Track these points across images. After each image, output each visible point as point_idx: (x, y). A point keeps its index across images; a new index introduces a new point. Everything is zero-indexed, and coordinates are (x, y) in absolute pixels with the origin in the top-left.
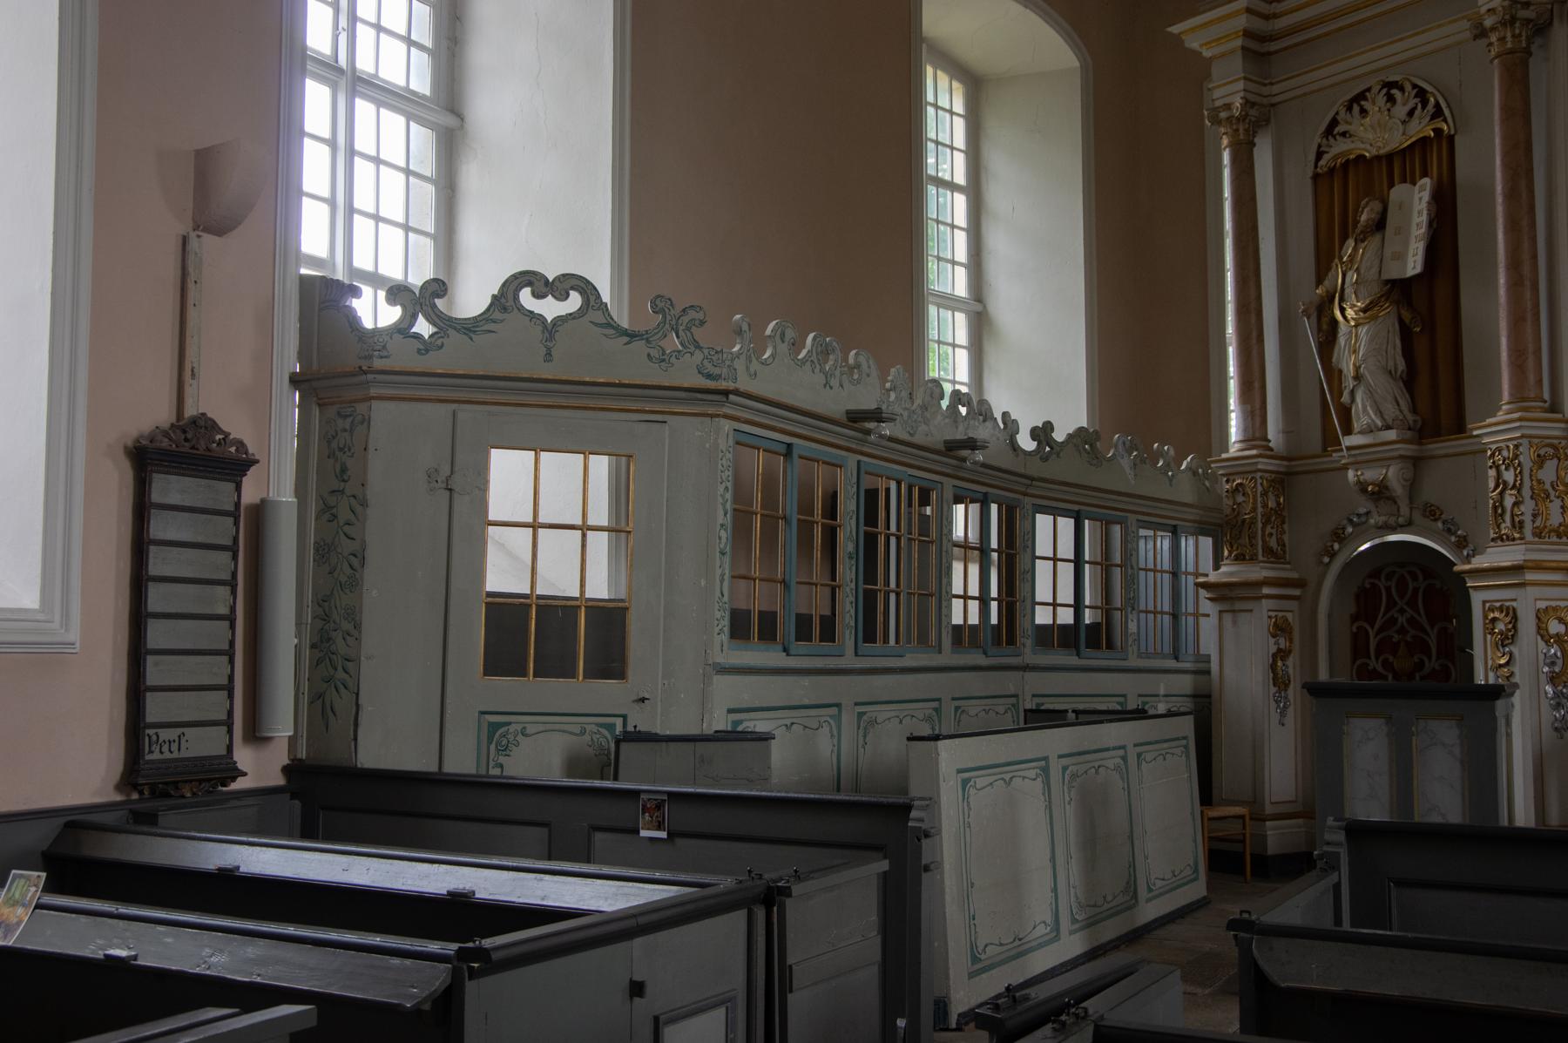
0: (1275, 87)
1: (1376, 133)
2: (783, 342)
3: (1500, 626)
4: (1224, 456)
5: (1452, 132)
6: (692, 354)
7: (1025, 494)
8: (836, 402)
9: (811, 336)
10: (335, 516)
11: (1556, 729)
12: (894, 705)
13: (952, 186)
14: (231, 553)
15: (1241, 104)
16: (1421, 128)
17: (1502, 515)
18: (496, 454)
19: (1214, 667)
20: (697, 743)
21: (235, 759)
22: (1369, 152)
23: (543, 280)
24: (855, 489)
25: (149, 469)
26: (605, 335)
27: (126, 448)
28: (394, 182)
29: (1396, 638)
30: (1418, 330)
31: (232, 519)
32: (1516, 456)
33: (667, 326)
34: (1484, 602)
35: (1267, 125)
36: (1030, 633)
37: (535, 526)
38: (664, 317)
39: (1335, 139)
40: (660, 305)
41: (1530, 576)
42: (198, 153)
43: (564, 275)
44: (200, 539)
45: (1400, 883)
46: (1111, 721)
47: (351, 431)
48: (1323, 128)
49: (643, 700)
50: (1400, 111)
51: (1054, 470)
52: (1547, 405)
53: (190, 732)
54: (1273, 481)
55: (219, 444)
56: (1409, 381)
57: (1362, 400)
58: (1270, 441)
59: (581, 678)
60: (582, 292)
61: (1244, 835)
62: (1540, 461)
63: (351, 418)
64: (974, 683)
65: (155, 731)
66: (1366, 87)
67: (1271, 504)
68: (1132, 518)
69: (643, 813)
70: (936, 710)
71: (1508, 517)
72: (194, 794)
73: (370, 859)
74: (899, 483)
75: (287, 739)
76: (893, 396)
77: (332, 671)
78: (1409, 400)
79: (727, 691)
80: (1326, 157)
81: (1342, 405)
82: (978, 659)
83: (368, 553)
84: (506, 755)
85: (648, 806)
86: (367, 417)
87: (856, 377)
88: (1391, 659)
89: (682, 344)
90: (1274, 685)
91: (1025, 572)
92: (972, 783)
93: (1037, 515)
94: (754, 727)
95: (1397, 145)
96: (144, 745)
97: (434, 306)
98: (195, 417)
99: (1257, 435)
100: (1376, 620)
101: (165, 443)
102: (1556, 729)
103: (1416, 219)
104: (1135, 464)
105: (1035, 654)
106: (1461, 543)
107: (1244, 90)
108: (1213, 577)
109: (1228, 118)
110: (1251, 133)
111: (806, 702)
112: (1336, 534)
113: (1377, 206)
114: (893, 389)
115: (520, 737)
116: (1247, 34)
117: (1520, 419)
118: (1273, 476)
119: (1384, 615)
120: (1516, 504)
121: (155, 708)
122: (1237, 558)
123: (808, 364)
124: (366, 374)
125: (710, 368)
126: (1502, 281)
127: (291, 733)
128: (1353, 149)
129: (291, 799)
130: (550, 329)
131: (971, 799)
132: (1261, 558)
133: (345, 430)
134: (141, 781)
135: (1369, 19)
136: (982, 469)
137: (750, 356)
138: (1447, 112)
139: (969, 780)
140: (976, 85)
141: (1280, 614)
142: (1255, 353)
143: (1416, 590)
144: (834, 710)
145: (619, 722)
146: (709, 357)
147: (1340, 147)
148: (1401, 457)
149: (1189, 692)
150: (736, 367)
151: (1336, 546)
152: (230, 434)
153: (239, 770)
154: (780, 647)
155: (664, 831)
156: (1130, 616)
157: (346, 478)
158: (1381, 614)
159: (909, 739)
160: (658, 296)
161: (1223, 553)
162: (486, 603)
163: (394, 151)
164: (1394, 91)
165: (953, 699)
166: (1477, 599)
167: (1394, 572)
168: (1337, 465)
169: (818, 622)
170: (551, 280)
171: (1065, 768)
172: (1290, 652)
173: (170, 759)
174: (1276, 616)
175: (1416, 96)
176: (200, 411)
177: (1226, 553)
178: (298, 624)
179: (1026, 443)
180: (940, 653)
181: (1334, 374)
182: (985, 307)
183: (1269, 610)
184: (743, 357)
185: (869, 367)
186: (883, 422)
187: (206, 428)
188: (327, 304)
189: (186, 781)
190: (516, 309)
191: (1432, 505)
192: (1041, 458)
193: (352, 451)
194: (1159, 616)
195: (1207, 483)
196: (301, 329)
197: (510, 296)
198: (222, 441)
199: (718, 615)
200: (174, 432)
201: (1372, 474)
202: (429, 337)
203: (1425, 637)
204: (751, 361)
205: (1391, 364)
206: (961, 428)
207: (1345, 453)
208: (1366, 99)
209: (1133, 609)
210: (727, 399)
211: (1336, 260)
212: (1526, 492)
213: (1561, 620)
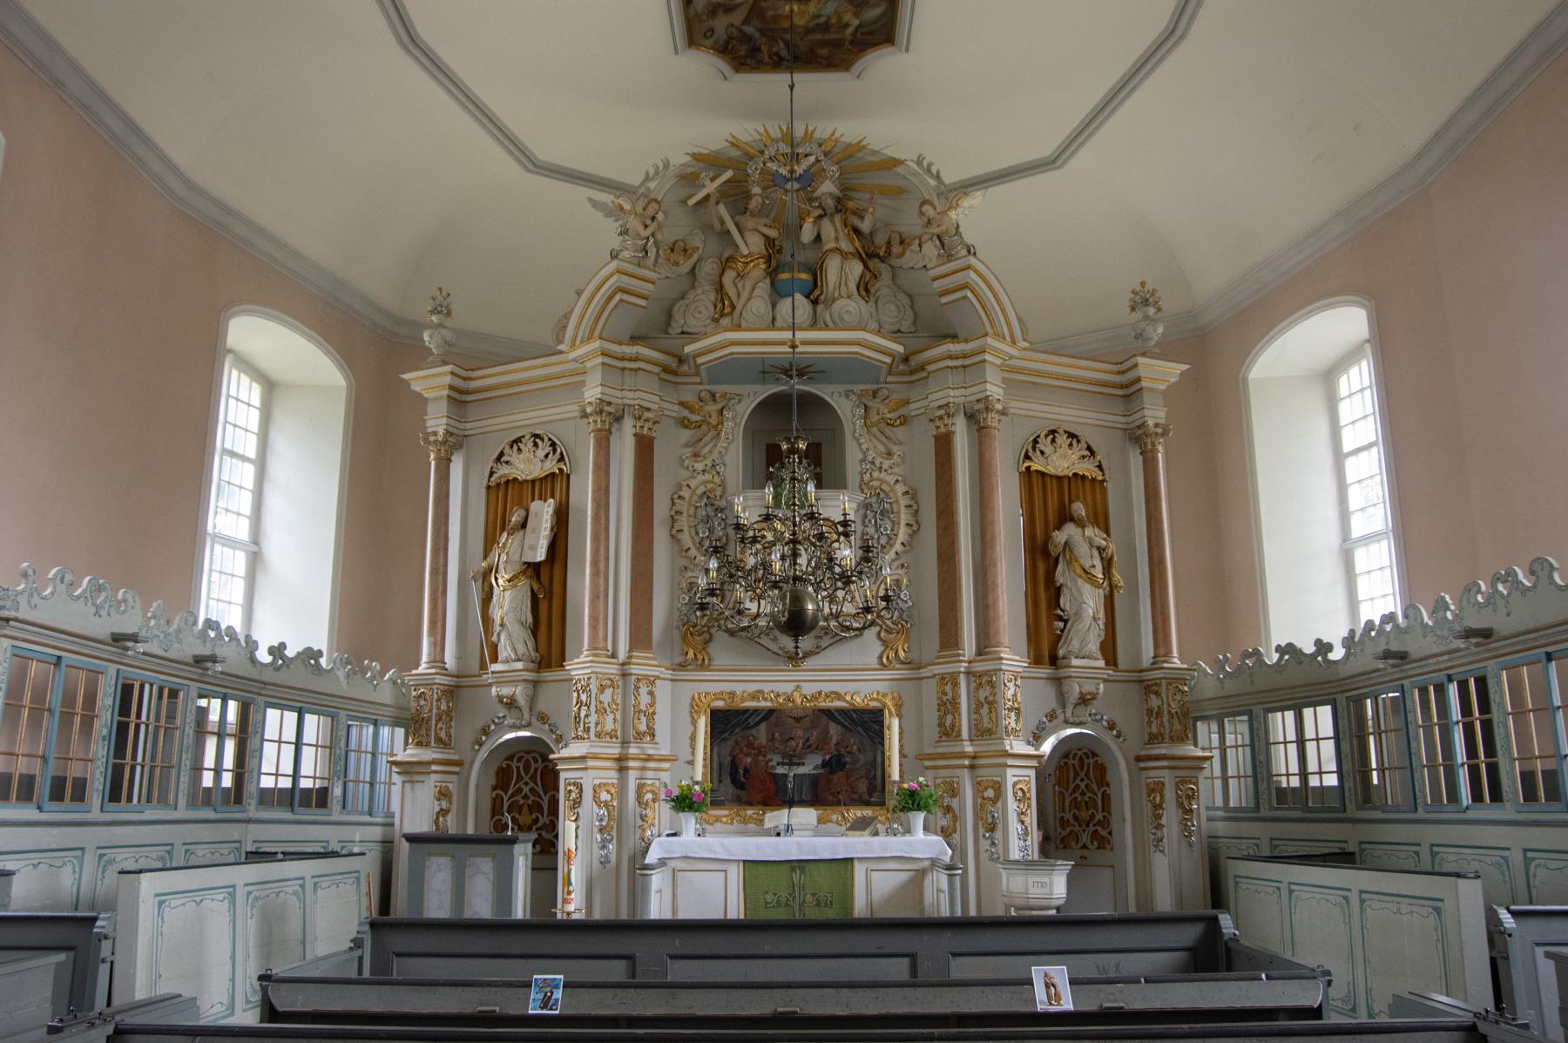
2: (62, 582)
3: (573, 795)
4: (414, 672)
7: (259, 694)
8: (102, 627)
9: (88, 579)
11: (601, 862)
13: (243, 458)
16: (551, 466)
17: (579, 723)
19: (397, 821)
24: (113, 690)
29: (521, 802)
32: (588, 685)
41: (591, 763)
45: (399, 955)
46: (293, 860)
48: (495, 456)
50: (541, 453)
51: (283, 677)
52: (609, 653)
56: (535, 631)
62: (602, 689)
64: (205, 832)
67: (443, 707)
68: (343, 713)
70: (168, 852)
71: (582, 724)
74: (152, 685)
76: (153, 622)
80: (495, 476)
81: (492, 642)
87: (122, 608)
88: (517, 816)
91: (255, 751)
92: (167, 903)
93: (268, 710)
99: (437, 659)
102: (601, 862)
104: (348, 675)
113: (522, 513)
114: (154, 617)
116: (451, 388)
117: (591, 662)
120: (586, 716)
126: (588, 571)
131: (165, 915)
135: (536, 390)
136: (221, 676)
139: (164, 901)
140: (270, 387)
142: (440, 602)
143: (536, 770)
144: (79, 853)
147: (503, 471)
148: (525, 680)
151: (484, 738)
154: (35, 805)
159: (120, 873)
164: (537, 440)
165: (184, 844)
166: (563, 776)
171: (249, 893)
172: (449, 811)
179: (264, 657)
180: (176, 809)
181: (487, 620)
182: (260, 548)
184: (26, 595)
185: (134, 602)
195: (404, 690)
201: (506, 691)
205: (523, 619)
206: (209, 646)
207: (490, 675)
208: (521, 442)
212: (593, 709)
213: (608, 792)
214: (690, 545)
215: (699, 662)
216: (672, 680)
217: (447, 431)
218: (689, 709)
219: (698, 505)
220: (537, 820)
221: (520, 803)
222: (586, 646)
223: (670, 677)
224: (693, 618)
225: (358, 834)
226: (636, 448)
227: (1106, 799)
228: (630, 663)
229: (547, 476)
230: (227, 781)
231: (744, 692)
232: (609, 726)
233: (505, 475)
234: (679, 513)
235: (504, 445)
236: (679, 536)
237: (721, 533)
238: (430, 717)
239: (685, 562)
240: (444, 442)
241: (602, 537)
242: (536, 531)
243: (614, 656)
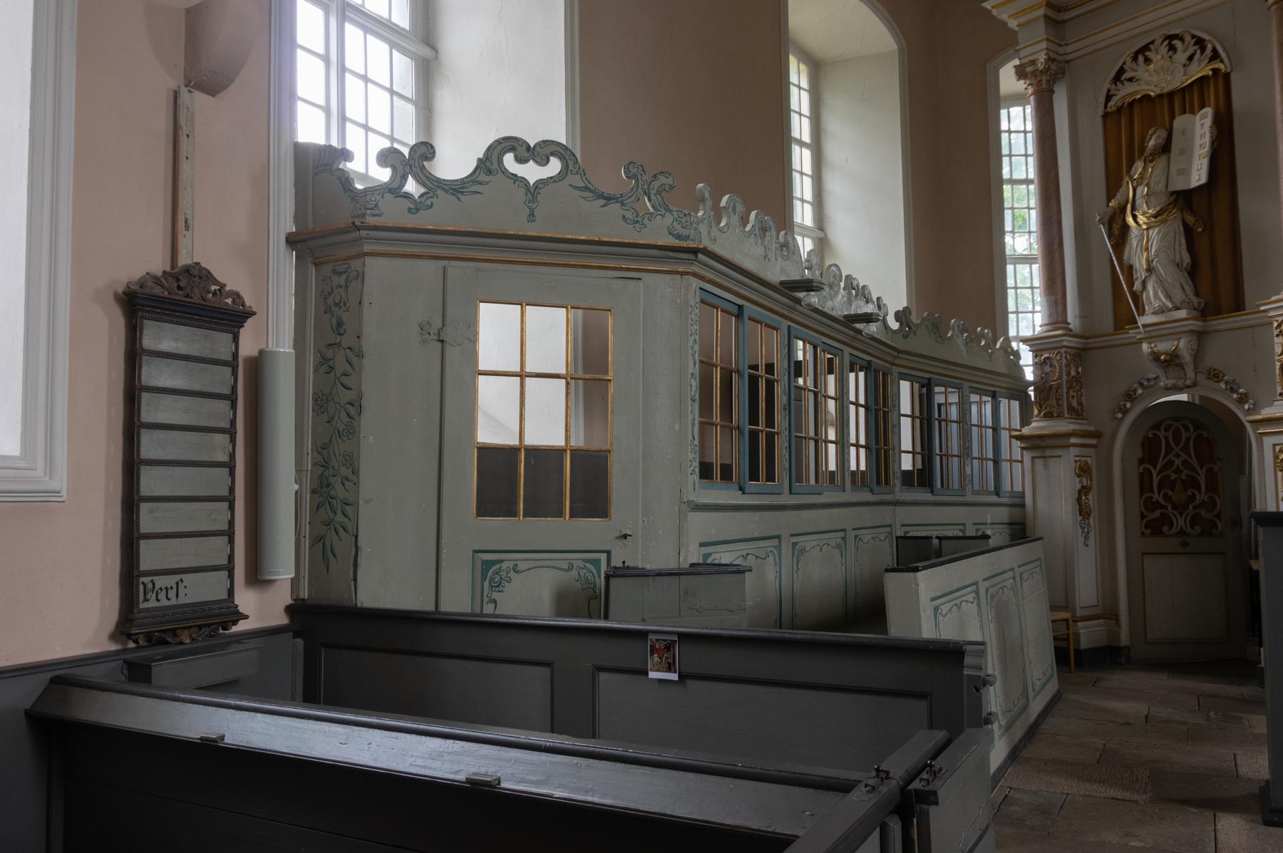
0: (1068, 47)
1: (1159, 76)
2: (735, 214)
5: (1229, 71)
6: (663, 216)
7: (894, 364)
10: (332, 368)
12: (809, 536)
14: (230, 402)
15: (1045, 59)
16: (1201, 69)
18: (483, 307)
20: (682, 577)
21: (236, 602)
22: (1153, 91)
23: (524, 145)
25: (140, 314)
26: (583, 198)
27: (116, 295)
28: (380, 100)
29: (1174, 476)
30: (1200, 230)
31: (230, 369)
33: (640, 190)
34: (1274, 445)
35: (1063, 77)
36: (898, 475)
37: (522, 375)
38: (637, 181)
39: (1123, 84)
40: (634, 170)
42: (188, 11)
43: (544, 142)
44: (196, 387)
47: (346, 287)
49: (625, 536)
50: (1181, 57)
53: (187, 578)
54: (1074, 355)
55: (214, 294)
57: (1154, 287)
58: (1069, 324)
59: (567, 518)
60: (562, 158)
61: (1068, 635)
63: (346, 274)
64: (867, 516)
65: (150, 578)
67: (1073, 373)
68: (966, 384)
69: (652, 654)
72: (193, 640)
73: (372, 730)
75: (289, 581)
77: (331, 515)
78: (1192, 286)
79: (701, 526)
80: (1115, 99)
82: (866, 496)
83: (364, 403)
84: (499, 591)
85: (657, 647)
86: (361, 274)
88: (1170, 493)
89: (653, 207)
90: (1080, 515)
94: (720, 558)
95: (1179, 84)
96: (138, 594)
97: (423, 168)
98: (190, 265)
100: (1157, 462)
101: (157, 291)
103: (1198, 142)
104: (967, 343)
105: (902, 492)
106: (1243, 399)
107: (1047, 49)
108: (1026, 431)
109: (1033, 72)
110: (1051, 83)
111: (757, 535)
112: (1128, 395)
113: (1163, 133)
115: (512, 574)
118: (1074, 351)
119: (1163, 459)
121: (150, 556)
122: (1045, 416)
123: (753, 236)
124: (359, 230)
125: (678, 229)
127: (293, 576)
128: (1140, 91)
129: (294, 638)
130: (532, 191)
132: (1066, 415)
133: (340, 286)
134: (134, 631)
137: (711, 223)
138: (1223, 55)
140: (816, 67)
141: (1083, 459)
144: (775, 542)
145: (603, 557)
146: (679, 219)
147: (1126, 92)
148: (1191, 331)
149: (1007, 521)
150: (701, 231)
151: (1128, 405)
152: (225, 285)
153: (240, 613)
154: (736, 486)
155: (675, 672)
156: (966, 462)
157: (342, 331)
158: (1161, 458)
160: (632, 163)
161: (1033, 412)
162: (477, 448)
163: (379, 73)
164: (1177, 43)
167: (1171, 425)
168: (1134, 340)
169: (764, 464)
170: (532, 146)
172: (1091, 488)
173: (167, 606)
174: (1080, 460)
175: (1195, 44)
176: (194, 261)
177: (1036, 412)
178: (299, 470)
180: (844, 491)
182: (826, 234)
183: (1075, 456)
186: (813, 291)
187: (200, 277)
188: (320, 169)
189: (185, 628)
190: (500, 173)
191: (1215, 370)
192: (903, 336)
193: (348, 305)
194: (984, 462)
196: (296, 193)
197: (495, 159)
198: (218, 292)
199: (691, 456)
200: (165, 279)
201: (1164, 346)
202: (419, 197)
203: (1195, 475)
204: (711, 227)
205: (1178, 260)
209: (968, 456)
210: (696, 257)
211: (1127, 179)
217: (1049, 58)
220: (1193, 498)
221: (1172, 478)
225: (989, 516)
227: (1145, 483)
230: (858, 460)
242: (1187, 152)
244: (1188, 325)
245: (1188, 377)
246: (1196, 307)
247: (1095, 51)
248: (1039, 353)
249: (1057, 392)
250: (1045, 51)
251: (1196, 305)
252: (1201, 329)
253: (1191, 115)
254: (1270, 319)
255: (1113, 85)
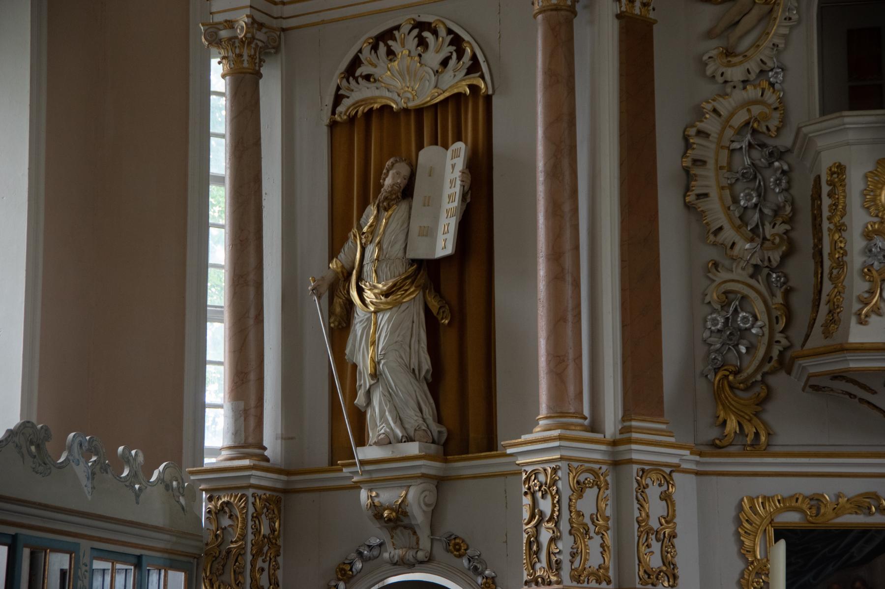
17: (537, 553)
32: (554, 482)
39: (357, 82)
50: (433, 58)
52: (586, 422)
54: (267, 500)
57: (380, 404)
58: (265, 449)
62: (580, 488)
66: (396, 24)
67: (265, 530)
68: (85, 545)
71: (543, 556)
78: (434, 405)
80: (346, 103)
95: (429, 99)
99: (251, 440)
103: (448, 190)
104: (93, 474)
109: (230, 39)
110: (257, 61)
112: (342, 570)
113: (404, 169)
118: (268, 493)
120: (553, 540)
126: (542, 272)
142: (252, 336)
148: (423, 476)
164: (426, 34)
175: (451, 44)
195: (182, 500)
201: (388, 497)
205: (414, 364)
207: (358, 468)
208: (394, 39)
211: (355, 230)
212: (565, 526)
214: (723, 221)
215: (749, 440)
216: (697, 473)
217: (254, 21)
218: (732, 528)
219: (736, 145)
222: (543, 410)
223: (693, 467)
224: (732, 357)
226: (621, 41)
228: (630, 441)
229: (446, 100)
231: (838, 496)
232: (594, 560)
233: (364, 101)
234: (699, 162)
235: (362, 42)
236: (702, 205)
237: (781, 199)
238: (243, 548)
239: (713, 254)
240: (248, 41)
241: (567, 207)
242: (433, 202)
243: (595, 427)
244: (420, 466)
245: (421, 547)
246: (436, 438)
247: (323, 22)
248: (216, 495)
249: (236, 562)
250: (248, 11)
251: (435, 435)
252: (441, 474)
253: (442, 149)
254: (519, 468)
255: (345, 80)
